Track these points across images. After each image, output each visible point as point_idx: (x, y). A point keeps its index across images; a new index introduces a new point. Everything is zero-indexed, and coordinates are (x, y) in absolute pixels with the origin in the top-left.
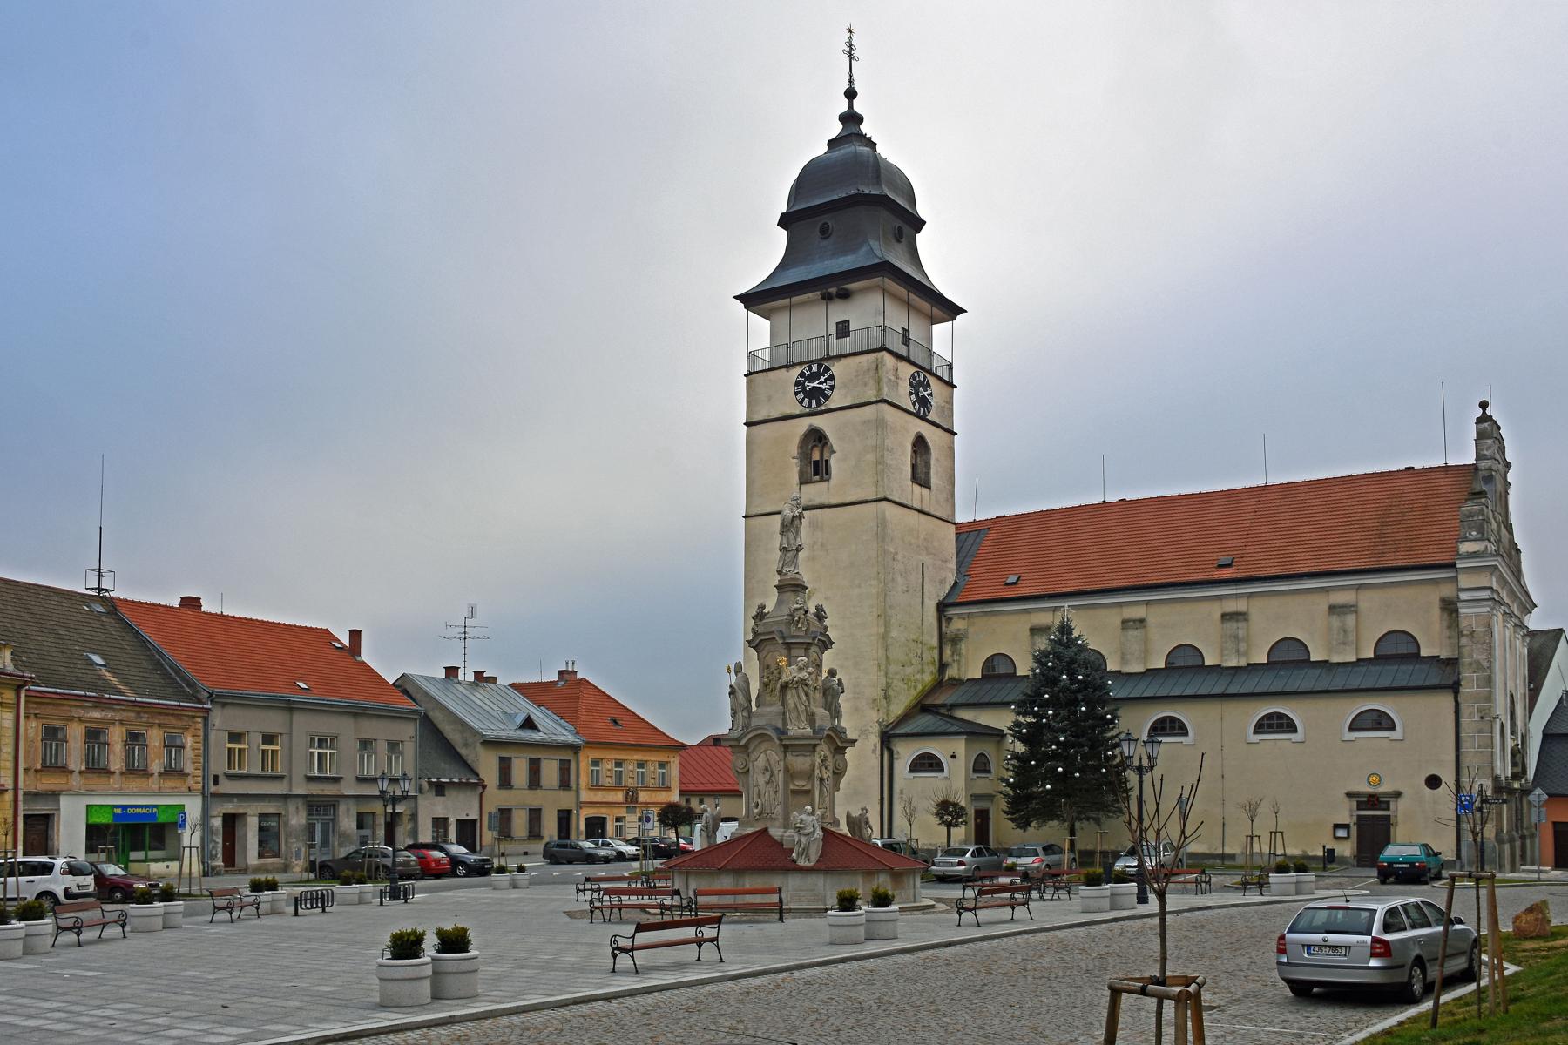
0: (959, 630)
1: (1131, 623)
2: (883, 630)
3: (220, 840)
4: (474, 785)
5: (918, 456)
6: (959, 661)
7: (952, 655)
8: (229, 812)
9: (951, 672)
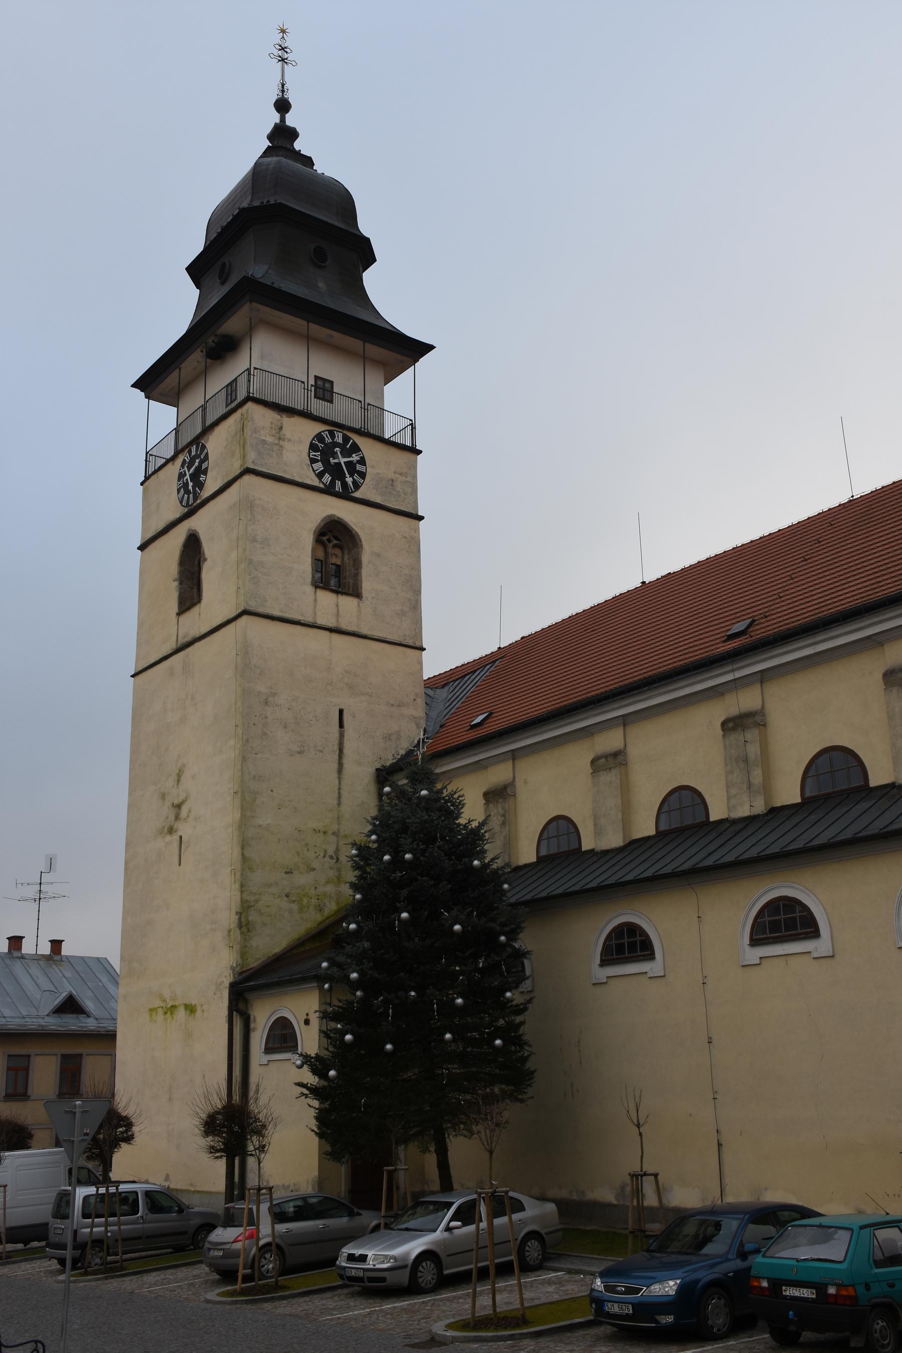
1: (603, 760)
5: (346, 552)
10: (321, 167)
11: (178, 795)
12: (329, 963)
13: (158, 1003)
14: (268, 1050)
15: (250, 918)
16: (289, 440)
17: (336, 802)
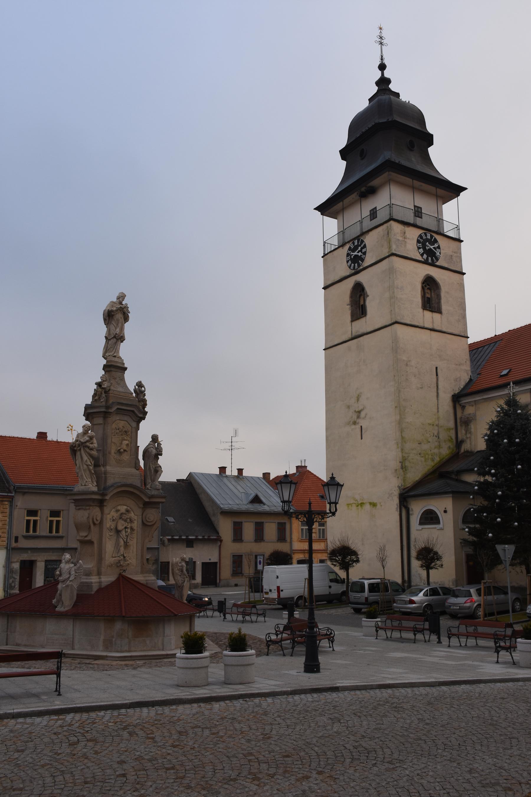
0: (470, 414)
2: (399, 418)
3: (18, 577)
4: (215, 540)
5: (433, 291)
6: (470, 438)
7: (466, 434)
8: (24, 559)
9: (466, 447)
10: (404, 98)
11: (358, 407)
12: (478, 487)
13: (352, 501)
14: (421, 523)
15: (406, 464)
16: (409, 238)
17: (436, 411)
